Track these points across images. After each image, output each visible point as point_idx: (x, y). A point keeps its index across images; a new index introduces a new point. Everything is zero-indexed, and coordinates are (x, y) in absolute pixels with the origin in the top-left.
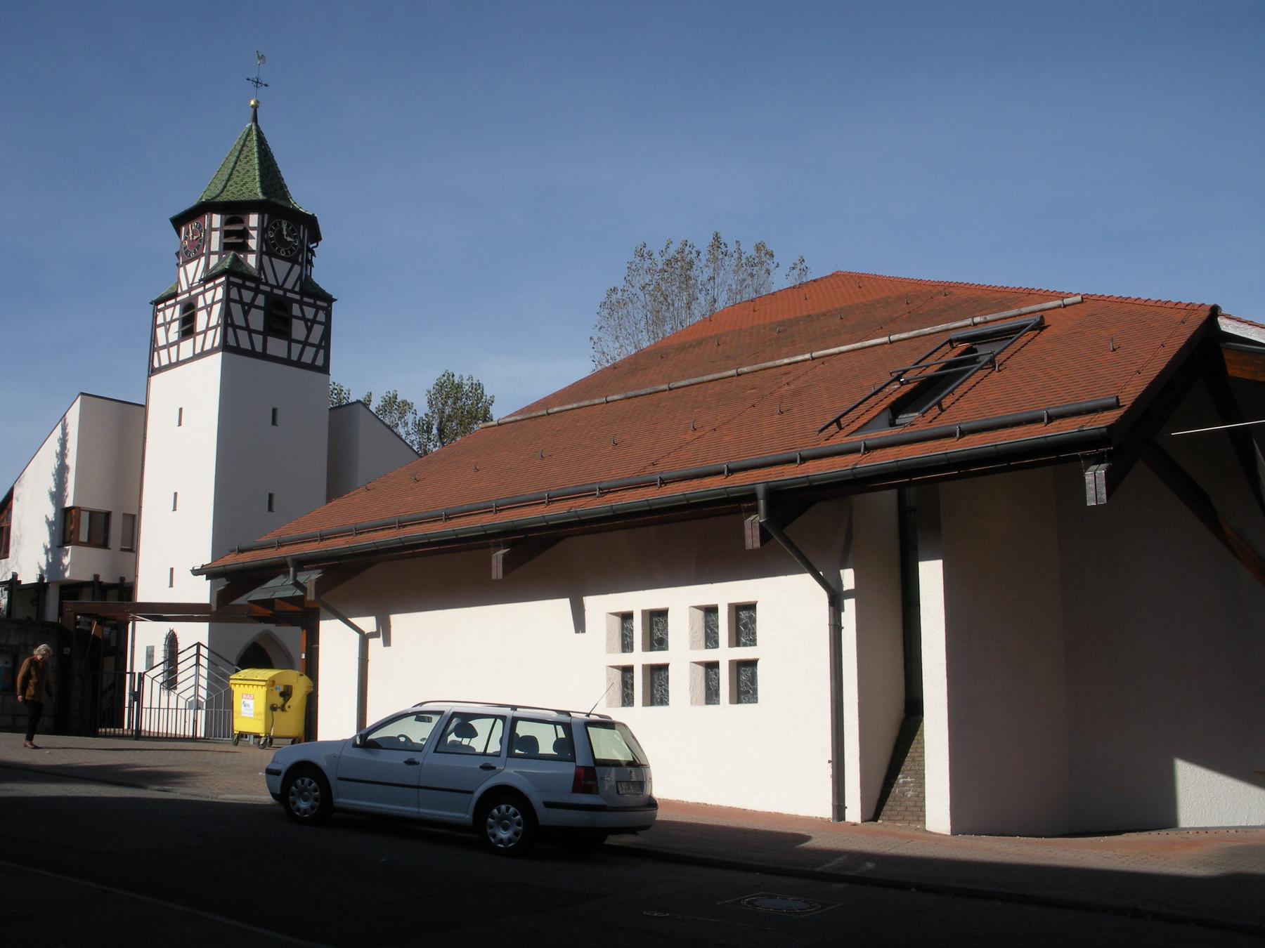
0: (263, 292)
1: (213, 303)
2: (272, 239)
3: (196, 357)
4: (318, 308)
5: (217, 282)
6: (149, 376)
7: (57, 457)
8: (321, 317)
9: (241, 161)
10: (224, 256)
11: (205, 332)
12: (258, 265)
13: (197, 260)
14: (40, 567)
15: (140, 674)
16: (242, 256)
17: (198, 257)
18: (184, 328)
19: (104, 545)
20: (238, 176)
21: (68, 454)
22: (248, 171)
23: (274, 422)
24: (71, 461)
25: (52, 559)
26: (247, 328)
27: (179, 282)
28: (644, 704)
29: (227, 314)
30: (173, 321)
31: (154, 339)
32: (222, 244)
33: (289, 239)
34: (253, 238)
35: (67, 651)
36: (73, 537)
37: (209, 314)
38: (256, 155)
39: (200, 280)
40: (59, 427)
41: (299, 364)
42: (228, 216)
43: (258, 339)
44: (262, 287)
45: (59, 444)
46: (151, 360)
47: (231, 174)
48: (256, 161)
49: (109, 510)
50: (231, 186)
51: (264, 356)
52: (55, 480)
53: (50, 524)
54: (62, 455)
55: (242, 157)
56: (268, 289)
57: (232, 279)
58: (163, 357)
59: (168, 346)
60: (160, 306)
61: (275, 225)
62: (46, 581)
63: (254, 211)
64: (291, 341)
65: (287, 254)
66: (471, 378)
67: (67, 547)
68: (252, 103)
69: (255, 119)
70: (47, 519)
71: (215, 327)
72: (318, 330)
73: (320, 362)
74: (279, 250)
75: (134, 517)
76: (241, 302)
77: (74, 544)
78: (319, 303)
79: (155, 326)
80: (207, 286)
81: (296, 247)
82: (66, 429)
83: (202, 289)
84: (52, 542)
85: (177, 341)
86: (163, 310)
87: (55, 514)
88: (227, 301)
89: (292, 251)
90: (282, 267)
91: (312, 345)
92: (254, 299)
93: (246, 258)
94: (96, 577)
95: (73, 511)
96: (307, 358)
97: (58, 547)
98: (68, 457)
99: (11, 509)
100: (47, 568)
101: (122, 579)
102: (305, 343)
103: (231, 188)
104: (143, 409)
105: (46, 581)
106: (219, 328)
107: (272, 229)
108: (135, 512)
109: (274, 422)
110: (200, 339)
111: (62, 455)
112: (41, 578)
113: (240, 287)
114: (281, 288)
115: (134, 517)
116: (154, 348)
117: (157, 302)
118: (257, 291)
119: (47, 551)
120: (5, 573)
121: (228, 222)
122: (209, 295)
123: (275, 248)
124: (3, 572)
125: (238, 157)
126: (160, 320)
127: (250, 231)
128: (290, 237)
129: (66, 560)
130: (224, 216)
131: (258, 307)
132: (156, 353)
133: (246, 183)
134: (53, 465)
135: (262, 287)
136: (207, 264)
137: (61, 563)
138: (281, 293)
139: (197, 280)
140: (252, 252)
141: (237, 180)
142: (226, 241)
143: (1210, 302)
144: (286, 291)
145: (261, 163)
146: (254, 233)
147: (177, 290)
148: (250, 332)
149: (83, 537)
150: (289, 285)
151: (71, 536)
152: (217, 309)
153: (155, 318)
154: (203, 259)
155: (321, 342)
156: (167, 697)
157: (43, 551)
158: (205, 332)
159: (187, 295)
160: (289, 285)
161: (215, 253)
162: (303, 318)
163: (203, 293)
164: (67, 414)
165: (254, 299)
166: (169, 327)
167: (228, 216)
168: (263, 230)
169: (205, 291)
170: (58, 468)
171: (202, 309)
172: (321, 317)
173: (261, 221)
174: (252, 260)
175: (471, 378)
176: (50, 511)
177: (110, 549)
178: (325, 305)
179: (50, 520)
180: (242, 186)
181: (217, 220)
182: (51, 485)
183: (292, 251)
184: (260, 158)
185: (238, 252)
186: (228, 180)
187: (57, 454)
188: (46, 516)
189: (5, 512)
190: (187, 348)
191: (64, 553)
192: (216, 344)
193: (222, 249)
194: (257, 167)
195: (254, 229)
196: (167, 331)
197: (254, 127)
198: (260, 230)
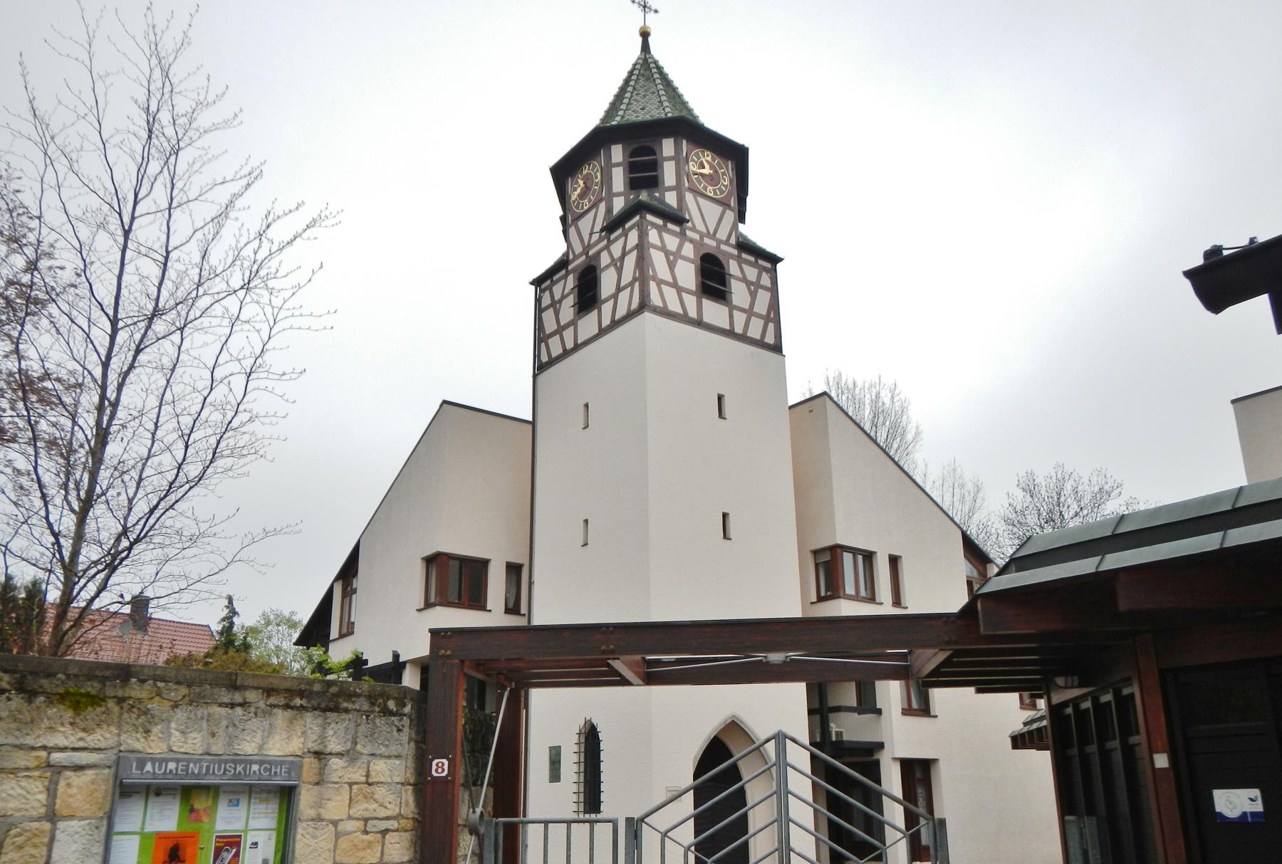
0: (691, 241)
1: (624, 254)
3: (602, 332)
5: (628, 225)
8: (766, 280)
11: (615, 296)
15: (629, 821)
26: (675, 285)
28: (484, 563)
30: (563, 297)
32: (628, 179)
37: (619, 271)
39: (602, 231)
41: (743, 338)
43: (690, 301)
51: (699, 323)
56: (697, 237)
59: (560, 330)
64: (732, 308)
65: (715, 193)
71: (631, 284)
72: (763, 298)
73: (770, 339)
74: (705, 188)
80: (613, 237)
83: (605, 242)
85: (573, 320)
92: (680, 247)
96: (755, 333)
106: (637, 284)
107: (693, 160)
109: (721, 414)
110: (607, 308)
114: (713, 236)
118: (682, 235)
121: (632, 155)
122: (616, 249)
131: (686, 259)
132: (543, 345)
136: (609, 210)
138: (714, 244)
139: (598, 227)
142: (631, 176)
143: (1231, 406)
144: (719, 242)
148: (680, 290)
155: (768, 313)
159: (584, 257)
160: (722, 234)
163: (607, 247)
165: (680, 247)
166: (560, 306)
169: (610, 242)
171: (607, 267)
178: (768, 265)
190: (589, 325)
196: (557, 314)
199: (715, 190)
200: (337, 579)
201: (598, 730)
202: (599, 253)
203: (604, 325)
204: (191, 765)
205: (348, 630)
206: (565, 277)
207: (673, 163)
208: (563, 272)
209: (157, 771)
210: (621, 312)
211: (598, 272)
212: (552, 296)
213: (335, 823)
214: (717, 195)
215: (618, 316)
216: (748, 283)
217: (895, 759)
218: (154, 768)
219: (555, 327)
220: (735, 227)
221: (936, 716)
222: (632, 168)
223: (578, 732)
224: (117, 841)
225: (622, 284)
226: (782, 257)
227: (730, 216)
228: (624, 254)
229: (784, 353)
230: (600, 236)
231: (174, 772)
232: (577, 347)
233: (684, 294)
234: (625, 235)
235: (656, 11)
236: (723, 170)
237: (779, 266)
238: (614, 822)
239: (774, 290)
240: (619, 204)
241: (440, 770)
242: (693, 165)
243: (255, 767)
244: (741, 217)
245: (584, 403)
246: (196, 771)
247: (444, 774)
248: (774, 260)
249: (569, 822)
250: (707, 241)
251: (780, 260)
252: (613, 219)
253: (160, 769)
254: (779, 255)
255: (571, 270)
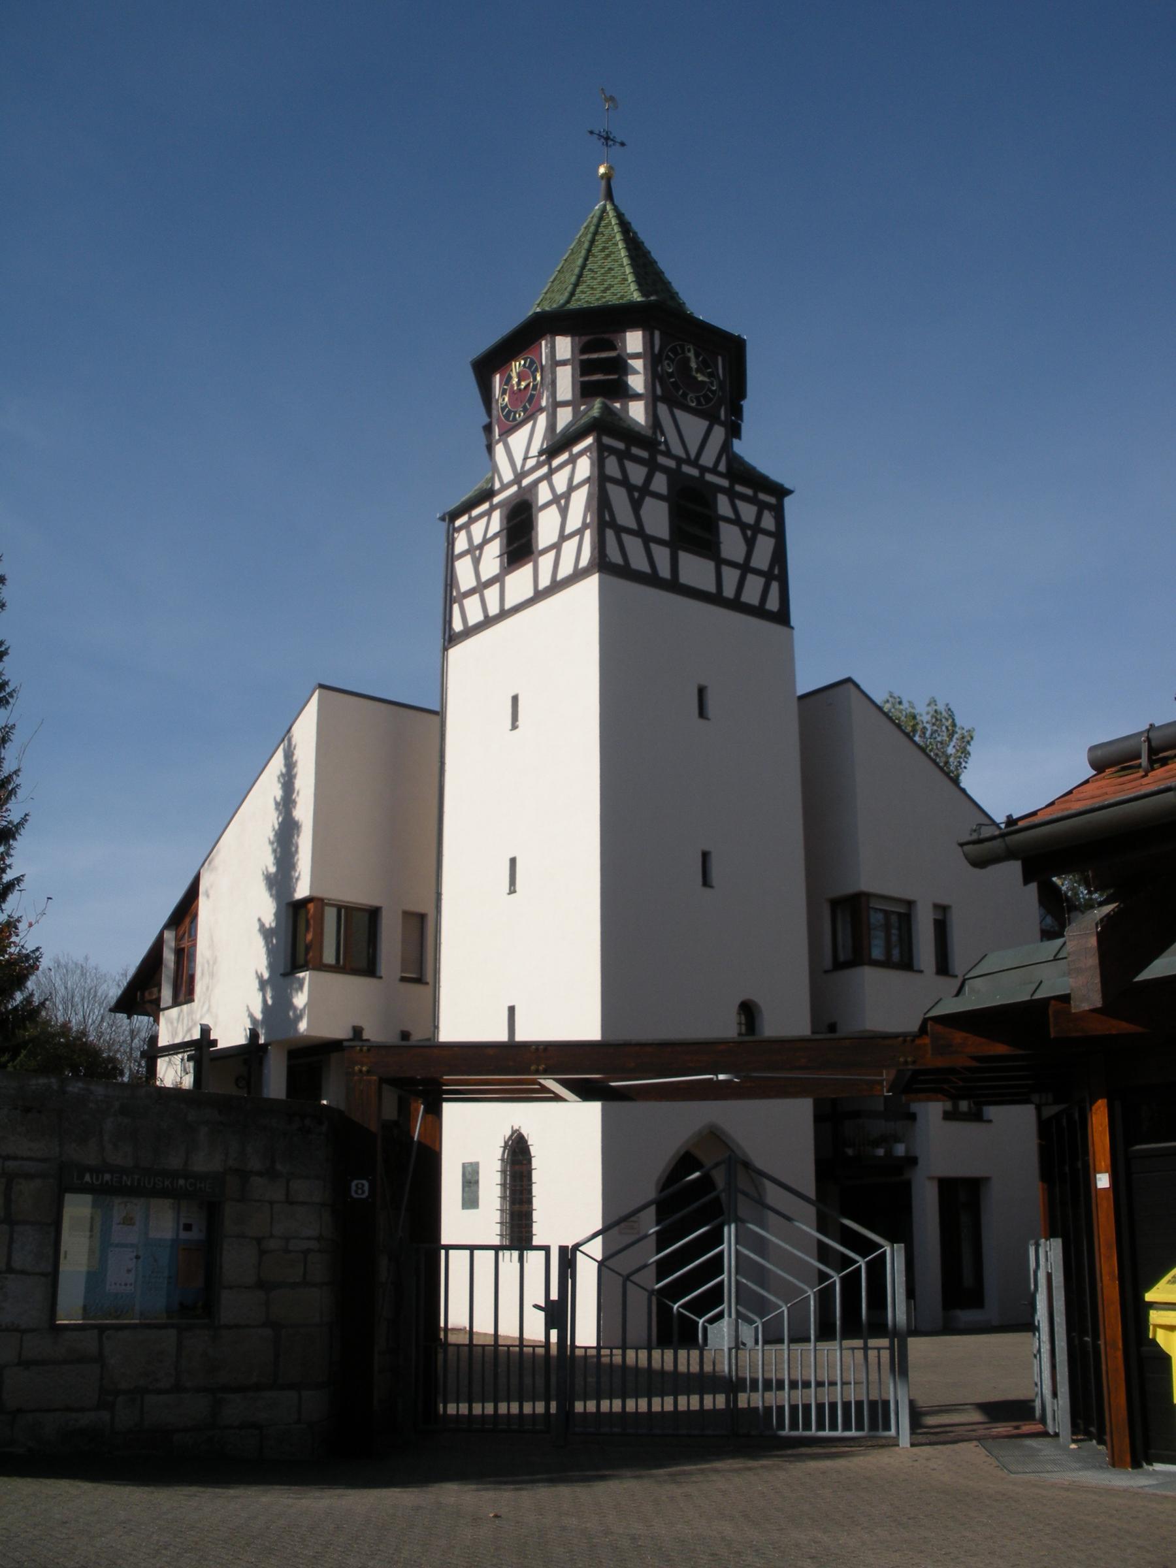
0: (665, 470)
1: (571, 488)
2: (671, 375)
3: (539, 595)
4: (762, 506)
5: (577, 449)
6: (445, 650)
7: (277, 809)
8: (768, 522)
9: (593, 256)
10: (583, 408)
11: (557, 547)
12: (651, 418)
13: (531, 423)
14: (251, 1016)
15: (563, 1250)
16: (618, 405)
17: (531, 417)
18: (511, 548)
19: (370, 969)
20: (593, 278)
21: (298, 800)
22: (611, 269)
23: (702, 713)
24: (304, 812)
25: (272, 997)
26: (640, 532)
27: (495, 469)
29: (601, 506)
30: (486, 541)
31: (450, 580)
33: (700, 378)
34: (636, 372)
35: (360, 1188)
36: (311, 954)
37: (564, 512)
38: (621, 245)
39: (541, 453)
40: (280, 755)
41: (736, 605)
42: (585, 339)
43: (662, 555)
44: (662, 460)
45: (280, 786)
46: (448, 621)
47: (580, 276)
48: (623, 253)
49: (374, 902)
50: (583, 292)
51: (674, 586)
52: (274, 851)
53: (267, 933)
54: (287, 803)
55: (595, 250)
56: (672, 464)
57: (607, 440)
58: (473, 611)
59: (481, 587)
60: (458, 523)
61: (674, 351)
62: (262, 1041)
63: (633, 326)
64: (720, 562)
65: (699, 403)
66: (933, 702)
67: (301, 975)
68: (602, 170)
69: (609, 196)
70: (262, 925)
71: (579, 532)
72: (764, 547)
73: (773, 604)
74: (685, 395)
75: (422, 917)
76: (624, 482)
77: (314, 969)
78: (762, 496)
79: (451, 558)
80: (556, 463)
81: (713, 392)
82: (293, 754)
83: (545, 469)
84: (271, 967)
86: (466, 526)
87: (277, 915)
88: (601, 481)
89: (708, 400)
90: (693, 426)
91: (758, 572)
92: (649, 479)
93: (625, 409)
94: (357, 1032)
95: (311, 906)
97: (285, 975)
98: (298, 806)
99: (195, 916)
100: (264, 1017)
101: (405, 1036)
102: (745, 568)
103: (583, 296)
104: (436, 719)
105: (262, 1041)
106: (588, 533)
107: (668, 357)
108: (428, 909)
109: (702, 713)
110: (546, 562)
111: (287, 803)
112: (254, 1035)
113: (622, 456)
114: (695, 463)
115: (422, 917)
116: (450, 594)
117: (454, 515)
118: (653, 467)
119: (263, 985)
120: (189, 1030)
121: (585, 349)
122: (560, 481)
123: (677, 392)
124: (185, 1028)
125: (589, 251)
126: (461, 544)
127: (630, 361)
128: (703, 374)
129: (300, 1000)
130: (577, 339)
132: (456, 607)
133: (611, 286)
134: (271, 825)
135: (662, 460)
137: (290, 1005)
138: (695, 472)
139: (534, 451)
140: (637, 397)
141: (595, 267)
144: (703, 470)
145: (631, 257)
146: (638, 364)
147: (493, 485)
148: (648, 540)
149: (329, 957)
150: (707, 460)
151: (307, 954)
152: (579, 499)
153: (451, 543)
154: (542, 419)
155: (771, 566)
156: (518, 1265)
157: (255, 984)
158: (557, 547)
160: (707, 460)
161: (565, 404)
162: (737, 521)
163: (548, 477)
164: (294, 728)
165: (649, 479)
166: (481, 554)
167: (585, 339)
168: (654, 359)
169: (552, 472)
170: (279, 828)
171: (547, 505)
172: (768, 522)
173: (648, 343)
174: (637, 412)
175: (933, 702)
176: (266, 909)
177: (381, 978)
178: (772, 500)
179: (267, 926)
180: (604, 291)
181: (564, 346)
182: (267, 861)
183: (708, 400)
184: (628, 249)
185: (610, 399)
186: (576, 285)
187: (277, 804)
188: (259, 920)
189: (187, 920)
190: (520, 583)
191: (296, 986)
192: (584, 561)
193: (579, 396)
194: (626, 261)
195: (636, 356)
196: (476, 562)
197: (609, 207)
198: (649, 356)
199: (698, 399)
200: (167, 926)
201: (529, 1143)
202: (536, 483)
203: (541, 586)
204: (125, 1178)
205: (184, 992)
206: (488, 513)
207: (614, 1350)
208: (485, 506)
209: (94, 1181)
210: (566, 570)
211: (534, 510)
212: (470, 539)
213: (259, 1240)
214: (702, 405)
215: (561, 575)
216: (743, 527)
217: (931, 1178)
218: (92, 1178)
219: (473, 583)
220: (726, 447)
221: (990, 1121)
222: (584, 368)
223: (503, 1145)
224: (1100, 1178)
225: (568, 531)
226: (792, 489)
227: (719, 433)
228: (571, 488)
229: (792, 624)
230: (538, 462)
231: (110, 1183)
232: (504, 614)
233: (653, 546)
234: (573, 460)
235: (623, 144)
236: (710, 370)
237: (787, 501)
238: (546, 1249)
239: (779, 535)
240: (565, 417)
241: (360, 1191)
242: (668, 365)
243: (181, 1182)
244: (734, 431)
245: (513, 694)
246: (129, 1183)
247: (364, 1196)
248: (781, 492)
249: (496, 1249)
250: (686, 469)
251: (789, 492)
252: (557, 438)
253: (97, 1179)
254: (788, 485)
255: (496, 504)
